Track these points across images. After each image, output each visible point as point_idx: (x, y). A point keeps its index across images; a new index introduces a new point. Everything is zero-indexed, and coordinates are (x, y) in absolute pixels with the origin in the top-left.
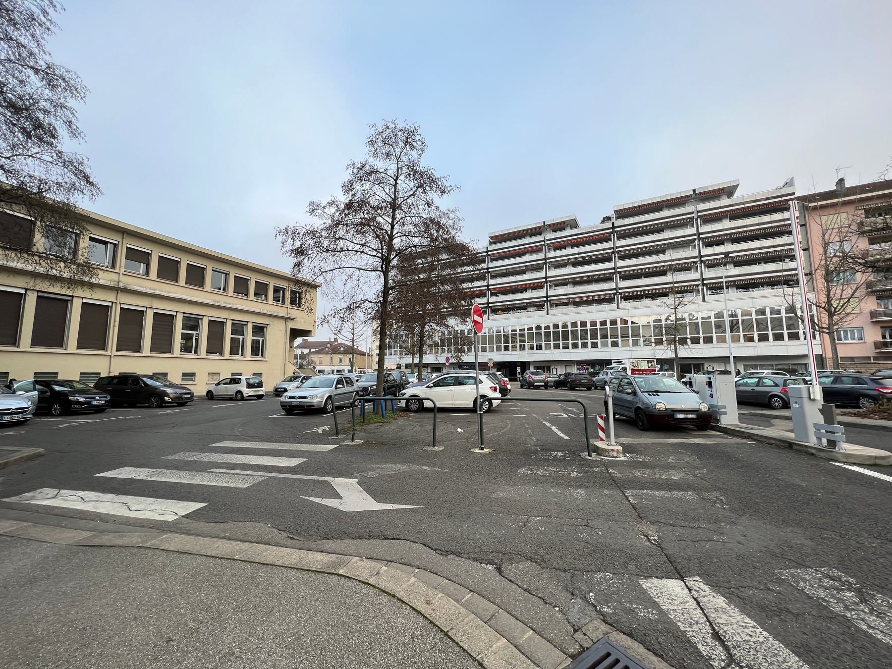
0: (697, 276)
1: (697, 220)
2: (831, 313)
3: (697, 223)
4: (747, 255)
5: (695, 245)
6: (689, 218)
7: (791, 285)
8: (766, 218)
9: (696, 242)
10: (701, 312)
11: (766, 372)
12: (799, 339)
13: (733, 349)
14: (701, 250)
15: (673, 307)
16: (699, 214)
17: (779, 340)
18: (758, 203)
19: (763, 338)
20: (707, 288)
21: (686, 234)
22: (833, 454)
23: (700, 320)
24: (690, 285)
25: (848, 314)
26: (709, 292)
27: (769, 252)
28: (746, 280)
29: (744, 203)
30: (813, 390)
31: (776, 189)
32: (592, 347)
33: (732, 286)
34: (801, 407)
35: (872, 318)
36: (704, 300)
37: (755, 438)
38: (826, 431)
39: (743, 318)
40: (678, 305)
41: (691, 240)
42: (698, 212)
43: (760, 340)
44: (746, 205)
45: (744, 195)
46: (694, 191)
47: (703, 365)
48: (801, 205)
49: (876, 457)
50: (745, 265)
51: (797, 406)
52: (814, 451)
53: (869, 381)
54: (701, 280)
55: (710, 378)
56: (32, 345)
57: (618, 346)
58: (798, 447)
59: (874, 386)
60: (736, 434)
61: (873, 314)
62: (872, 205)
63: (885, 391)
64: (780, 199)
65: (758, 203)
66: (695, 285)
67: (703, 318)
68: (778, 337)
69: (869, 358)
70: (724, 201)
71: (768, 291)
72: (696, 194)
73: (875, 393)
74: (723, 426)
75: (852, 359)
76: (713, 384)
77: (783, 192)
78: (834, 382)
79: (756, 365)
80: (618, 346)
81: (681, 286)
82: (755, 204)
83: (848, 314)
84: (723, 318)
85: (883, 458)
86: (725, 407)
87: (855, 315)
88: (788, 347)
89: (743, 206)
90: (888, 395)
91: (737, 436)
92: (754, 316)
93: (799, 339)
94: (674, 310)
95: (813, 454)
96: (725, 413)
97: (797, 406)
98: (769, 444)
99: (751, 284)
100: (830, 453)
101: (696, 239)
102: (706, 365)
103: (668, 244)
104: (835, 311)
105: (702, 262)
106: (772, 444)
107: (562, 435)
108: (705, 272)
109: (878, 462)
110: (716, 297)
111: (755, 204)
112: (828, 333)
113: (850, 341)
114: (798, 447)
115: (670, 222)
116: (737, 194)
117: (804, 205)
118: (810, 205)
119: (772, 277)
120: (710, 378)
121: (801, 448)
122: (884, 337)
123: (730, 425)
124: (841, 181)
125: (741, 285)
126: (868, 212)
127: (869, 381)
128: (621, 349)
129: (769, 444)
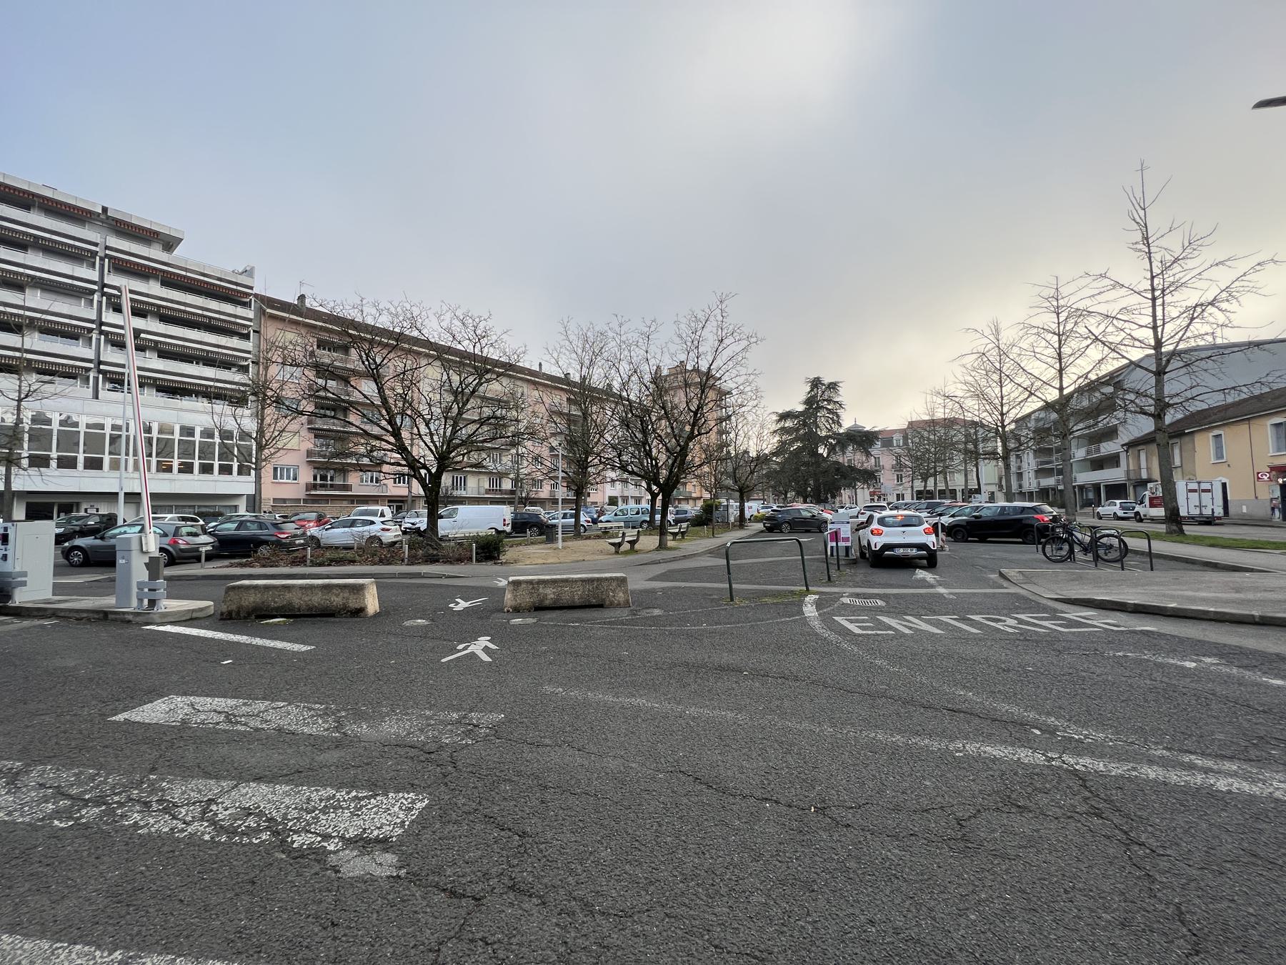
0: (89, 353)
1: (102, 259)
2: (261, 446)
3: (102, 266)
4: (179, 346)
5: (92, 300)
6: (89, 251)
7: (234, 403)
8: (214, 304)
9: (96, 297)
10: (88, 415)
11: (169, 516)
12: (101, 469)
13: (124, 482)
14: (104, 314)
15: (15, 396)
16: (107, 252)
17: (208, 473)
18: (206, 279)
19: (186, 469)
20: (105, 379)
21: (76, 275)
22: (151, 615)
23: (82, 429)
24: (76, 367)
25: (279, 449)
26: (108, 386)
27: (212, 352)
28: (173, 381)
29: (186, 270)
30: (146, 540)
31: (233, 271)
32: (86, 468)
33: (150, 385)
34: (129, 562)
35: (307, 457)
36: (96, 396)
37: (62, 614)
38: (149, 590)
39: (159, 436)
40: (27, 396)
41: (86, 289)
42: (107, 248)
43: (180, 471)
44: (189, 274)
45: (187, 257)
46: (105, 210)
47: (78, 505)
48: (258, 306)
49: (193, 611)
50: (175, 359)
51: (124, 561)
52: (130, 617)
53: (270, 526)
54: (96, 362)
55: (6, 529)
56: (54, 575)
57: (192, 472)
58: (113, 616)
59: (273, 531)
60: (35, 613)
61: (309, 453)
62: (325, 336)
63: (282, 536)
64: (234, 287)
65: (206, 279)
66: (82, 368)
67: (88, 426)
68: (207, 469)
69: (299, 500)
70: (155, 252)
71: (202, 404)
72: (108, 217)
73: (274, 538)
74: (17, 604)
75: (284, 500)
76: (11, 538)
77: (240, 279)
78: (238, 529)
79: (171, 506)
80: (192, 472)
81: (46, 362)
82: (202, 278)
83: (279, 449)
84: (173, 433)
85: (201, 610)
86: (25, 574)
87: (285, 451)
88: (218, 483)
89: (184, 273)
90: (284, 541)
91: (35, 617)
92: (177, 436)
93: (101, 469)
94: (16, 403)
95: (129, 622)
96: (24, 584)
97: (124, 561)
98: (77, 619)
99: (180, 389)
100: (147, 616)
101: (95, 291)
102: (84, 506)
103: (33, 277)
104: (266, 445)
105: (101, 332)
106: (81, 619)
107: (297, 647)
108: (105, 350)
109: (195, 615)
110: (117, 396)
111: (202, 278)
112: (255, 469)
113: (285, 481)
114: (113, 616)
115: (43, 238)
116: (178, 251)
117: (261, 308)
118: (269, 310)
119: (159, 379)
120: (6, 529)
121: (118, 616)
122: (315, 478)
123: (33, 602)
124: (302, 298)
125: (164, 386)
126: (321, 344)
127: (270, 526)
128: (196, 478)
129: (77, 619)
